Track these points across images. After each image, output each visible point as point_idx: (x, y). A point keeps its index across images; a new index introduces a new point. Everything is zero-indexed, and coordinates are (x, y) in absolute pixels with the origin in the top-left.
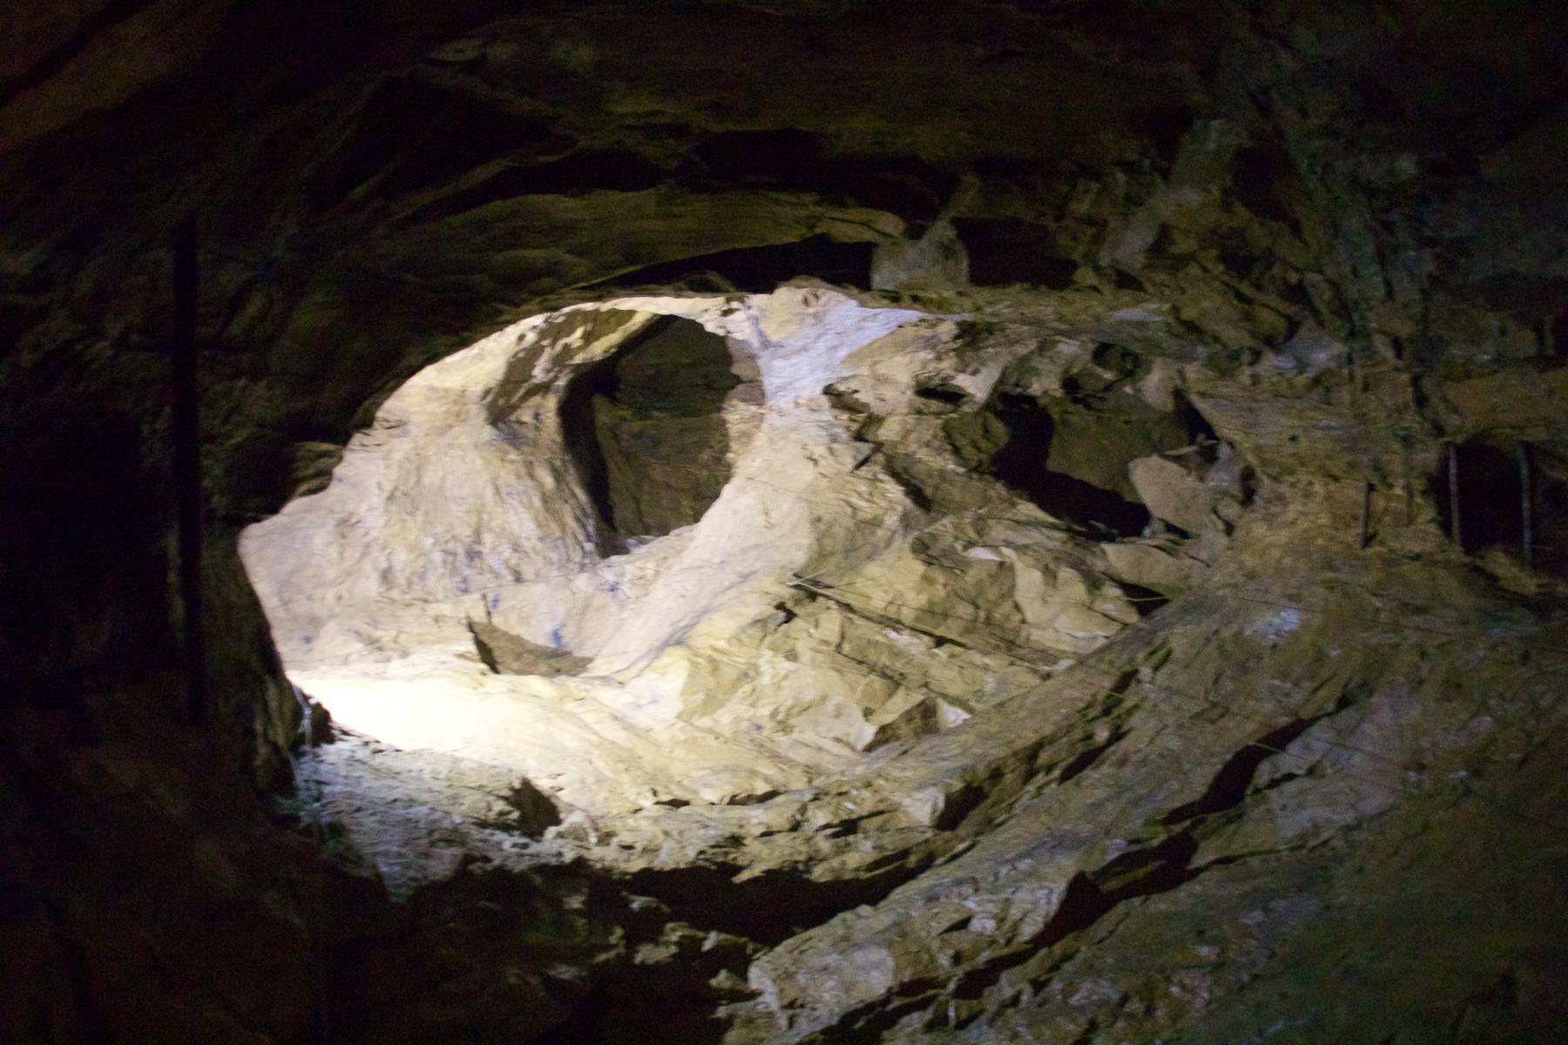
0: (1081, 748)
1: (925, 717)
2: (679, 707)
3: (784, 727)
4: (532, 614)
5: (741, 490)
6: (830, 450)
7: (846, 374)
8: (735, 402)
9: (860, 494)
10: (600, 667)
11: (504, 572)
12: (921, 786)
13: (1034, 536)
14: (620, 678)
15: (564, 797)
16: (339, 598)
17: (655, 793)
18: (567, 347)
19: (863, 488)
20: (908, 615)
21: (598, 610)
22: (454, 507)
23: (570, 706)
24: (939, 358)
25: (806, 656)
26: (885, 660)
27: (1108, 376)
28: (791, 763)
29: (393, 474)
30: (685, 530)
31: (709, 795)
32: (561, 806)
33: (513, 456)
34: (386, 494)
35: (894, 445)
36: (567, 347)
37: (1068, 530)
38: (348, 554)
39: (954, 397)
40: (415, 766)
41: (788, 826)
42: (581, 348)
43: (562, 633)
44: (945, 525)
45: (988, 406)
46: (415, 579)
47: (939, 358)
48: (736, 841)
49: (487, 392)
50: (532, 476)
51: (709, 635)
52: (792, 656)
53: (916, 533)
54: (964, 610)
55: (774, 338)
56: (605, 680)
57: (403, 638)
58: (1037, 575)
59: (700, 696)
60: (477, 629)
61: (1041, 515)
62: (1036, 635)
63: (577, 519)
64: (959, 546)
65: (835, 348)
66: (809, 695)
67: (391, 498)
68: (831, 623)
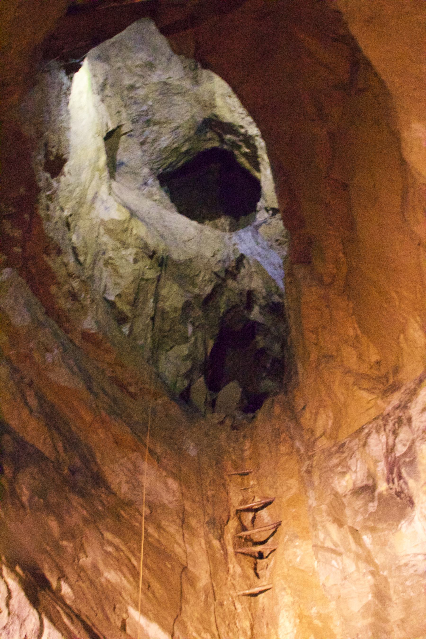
0: (125, 383)
1: (122, 319)
2: (106, 219)
3: (106, 264)
4: (130, 153)
5: (196, 228)
6: (219, 261)
7: (251, 262)
8: (229, 220)
9: (204, 277)
10: (114, 184)
11: (144, 137)
12: (97, 322)
13: (201, 349)
14: (112, 193)
15: (62, 178)
16: (119, 68)
17: (71, 215)
18: (240, 147)
19: (207, 277)
20: (160, 304)
21: (136, 179)
22: (167, 111)
23: (97, 174)
24: (264, 298)
25: (137, 266)
26: (141, 299)
27: (268, 365)
28: (93, 269)
29: (176, 83)
30: (174, 209)
31: (74, 238)
32: (58, 178)
33: (192, 132)
34: (167, 81)
35: (226, 286)
36: (240, 147)
37: (206, 361)
38: (139, 69)
39: (249, 307)
40: (63, 112)
41: (70, 272)
42: (241, 152)
43: (124, 166)
44: (198, 312)
45: (248, 320)
46: (133, 100)
47: (264, 298)
48: (59, 252)
49: (216, 116)
50: (185, 142)
51: (137, 227)
52: (136, 261)
53: (193, 302)
54: (167, 327)
55: (261, 230)
56: (110, 188)
57: (108, 99)
58: (186, 352)
59: (112, 227)
60: (118, 129)
61: (210, 350)
62: (163, 357)
63: (171, 163)
64: (191, 319)
65: (260, 256)
66: (121, 271)
67: (166, 84)
68: (151, 274)
